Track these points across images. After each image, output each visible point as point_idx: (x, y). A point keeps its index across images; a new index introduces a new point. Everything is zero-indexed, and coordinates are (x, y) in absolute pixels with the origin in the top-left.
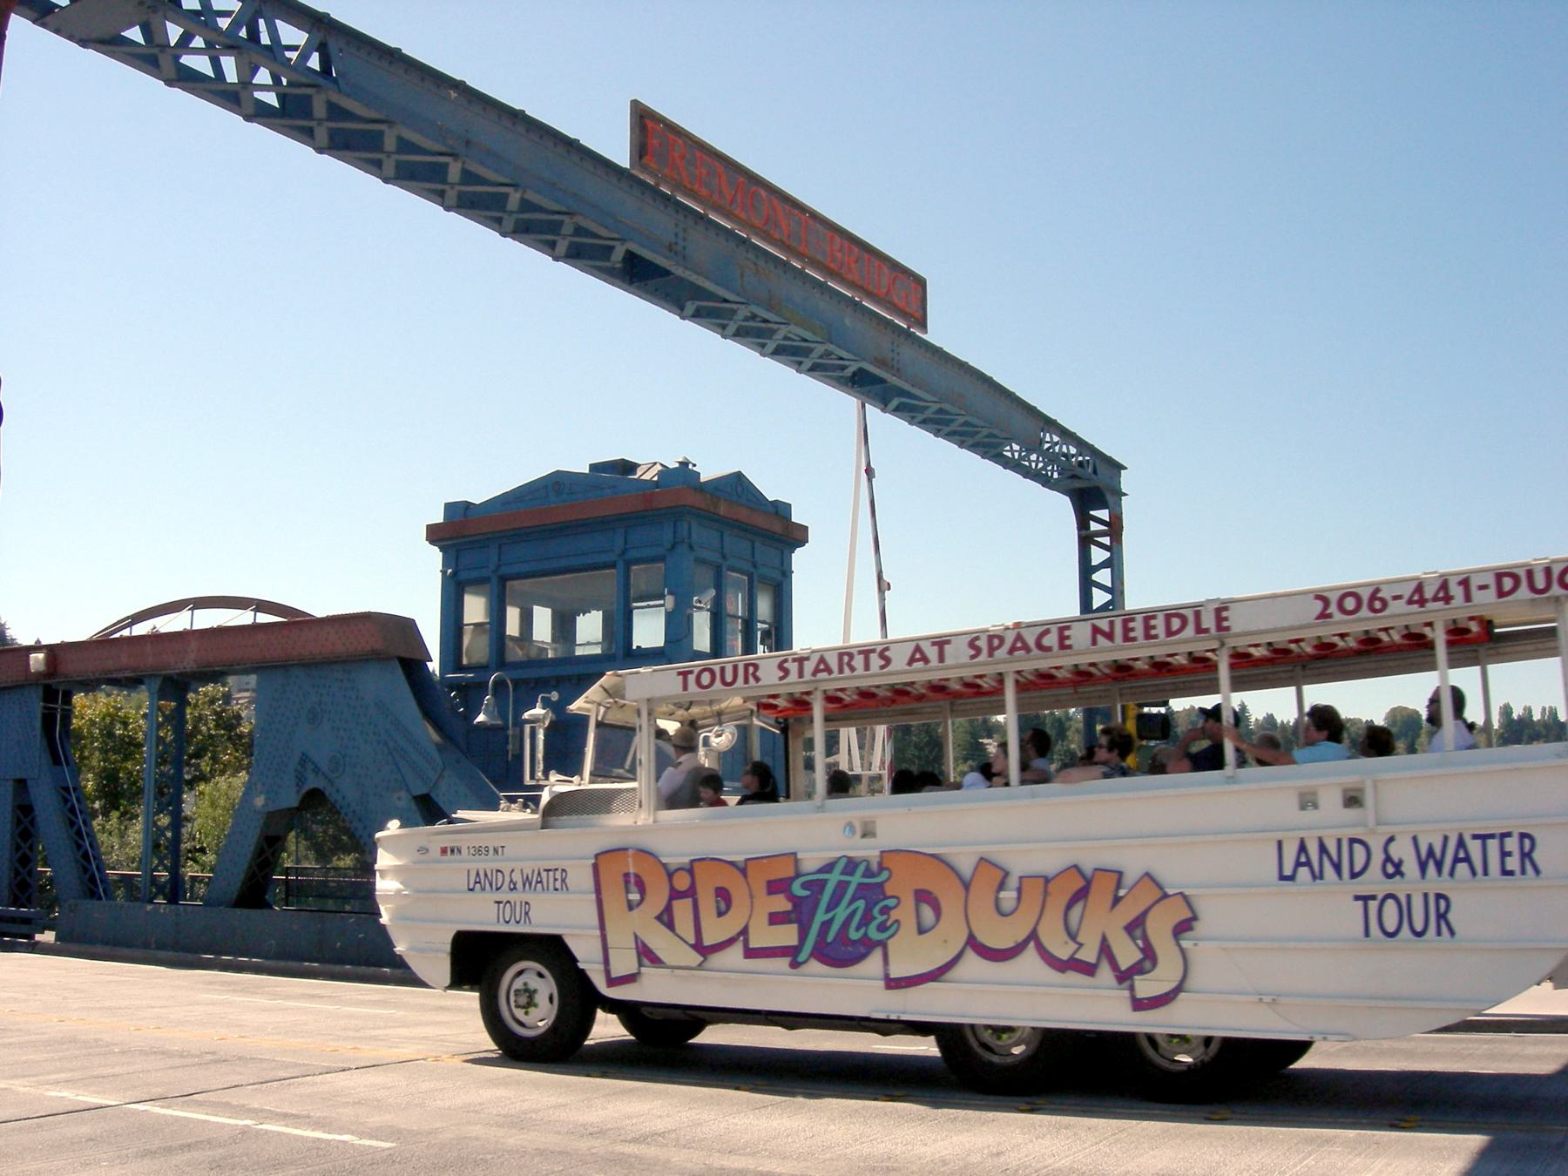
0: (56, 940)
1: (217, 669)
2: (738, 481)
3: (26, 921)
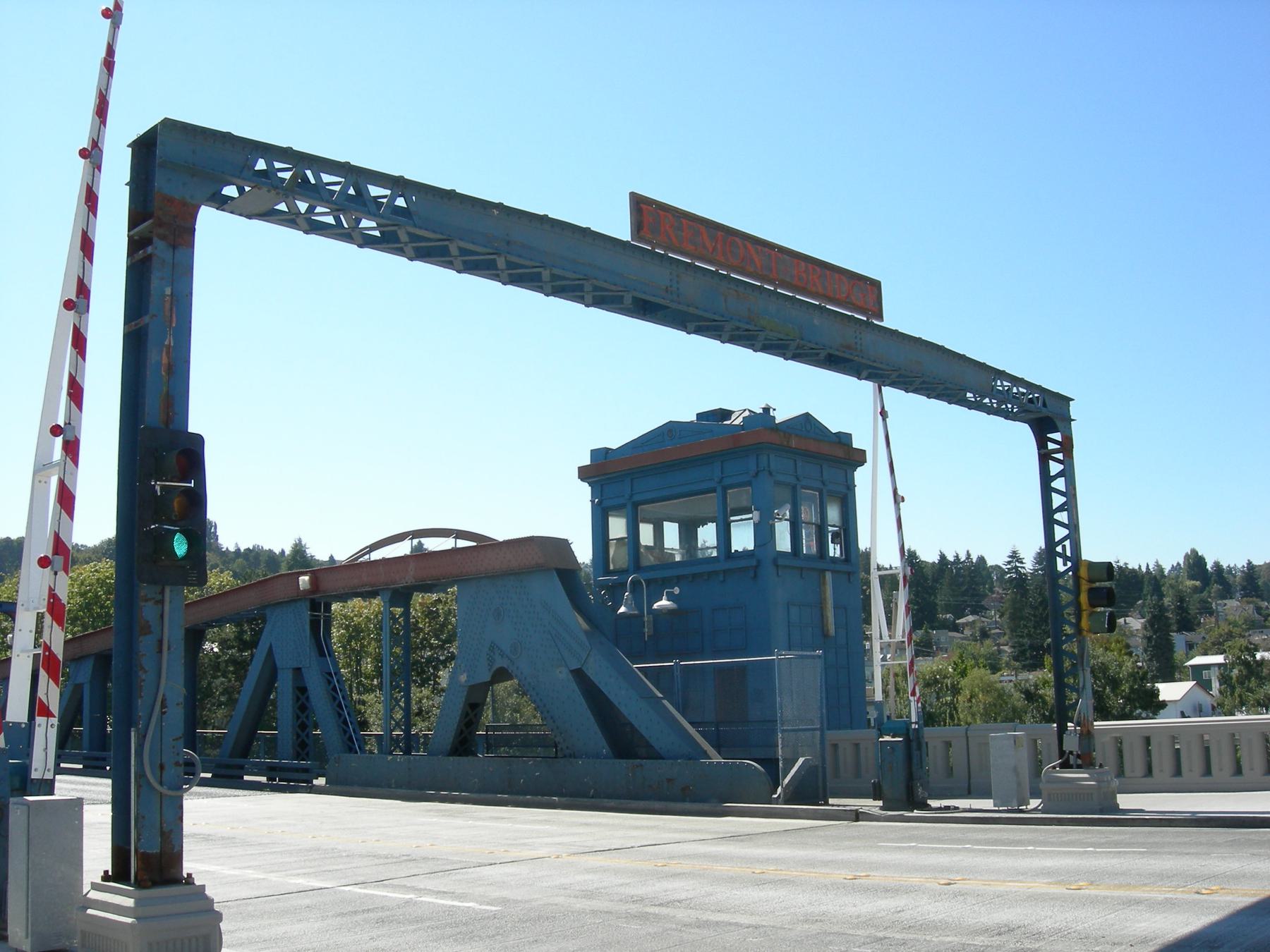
0: (326, 783)
1: (429, 582)
2: (807, 418)
3: (306, 770)
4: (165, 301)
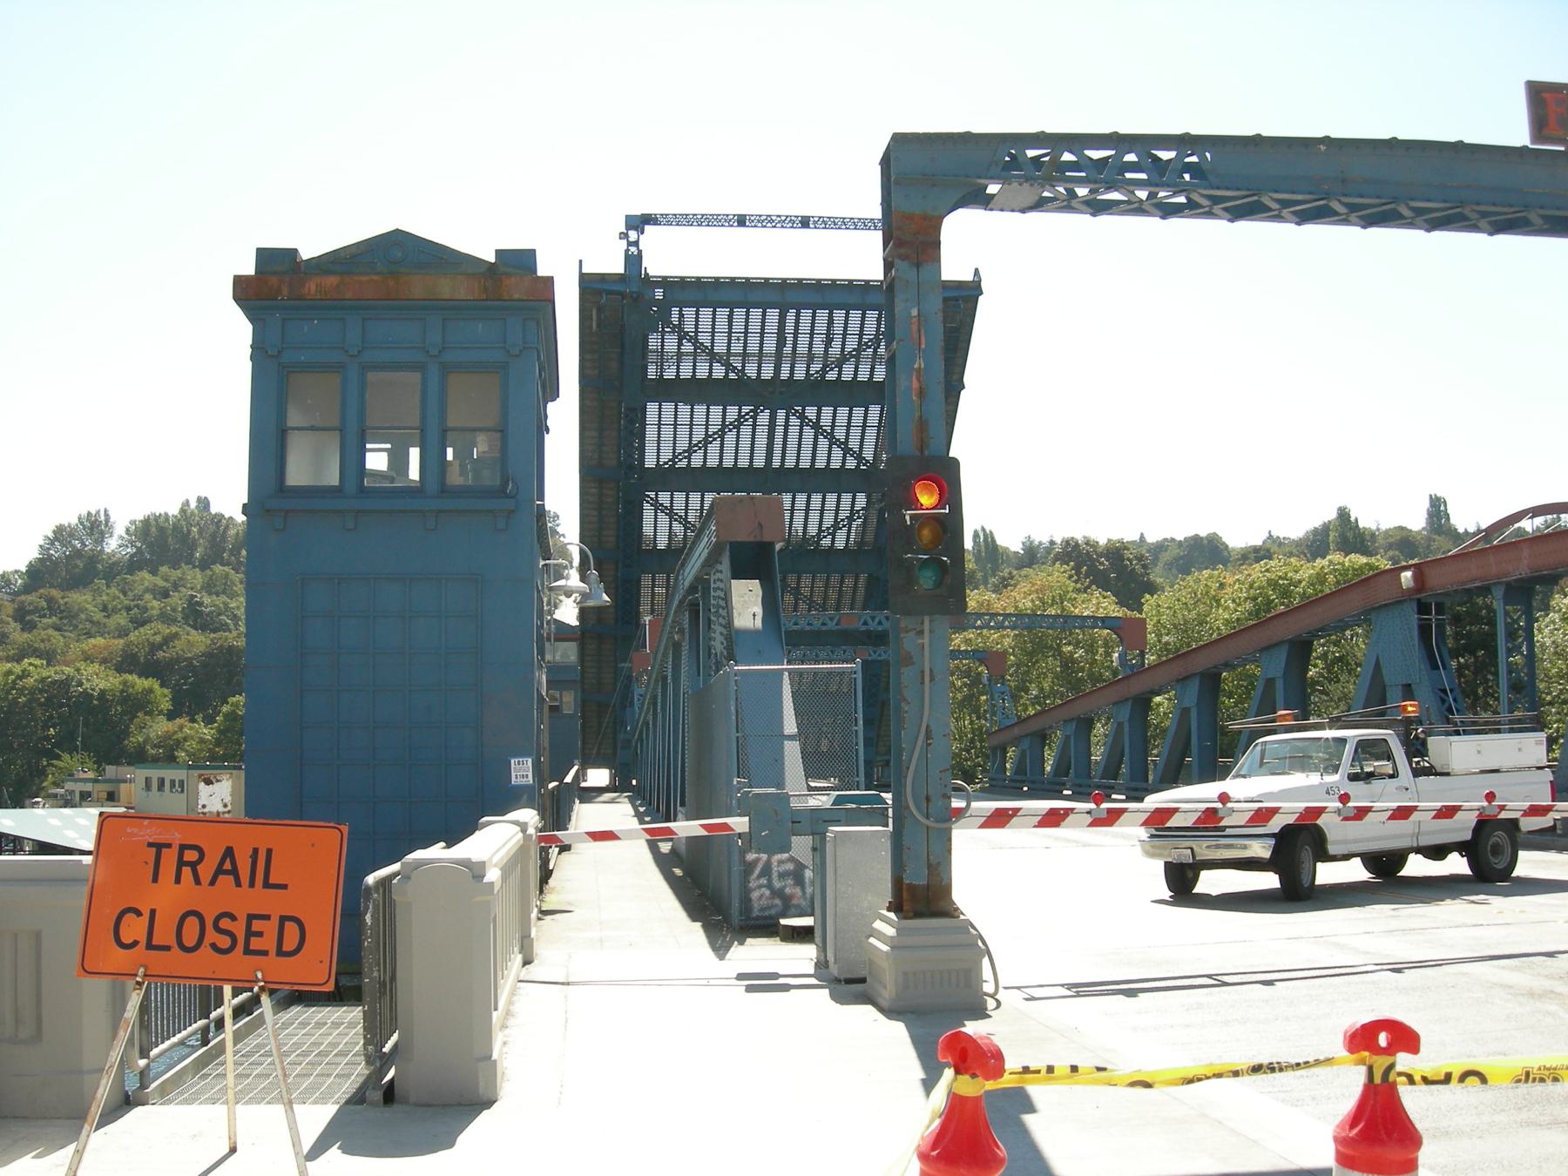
1: (1546, 572)
4: (911, 323)
